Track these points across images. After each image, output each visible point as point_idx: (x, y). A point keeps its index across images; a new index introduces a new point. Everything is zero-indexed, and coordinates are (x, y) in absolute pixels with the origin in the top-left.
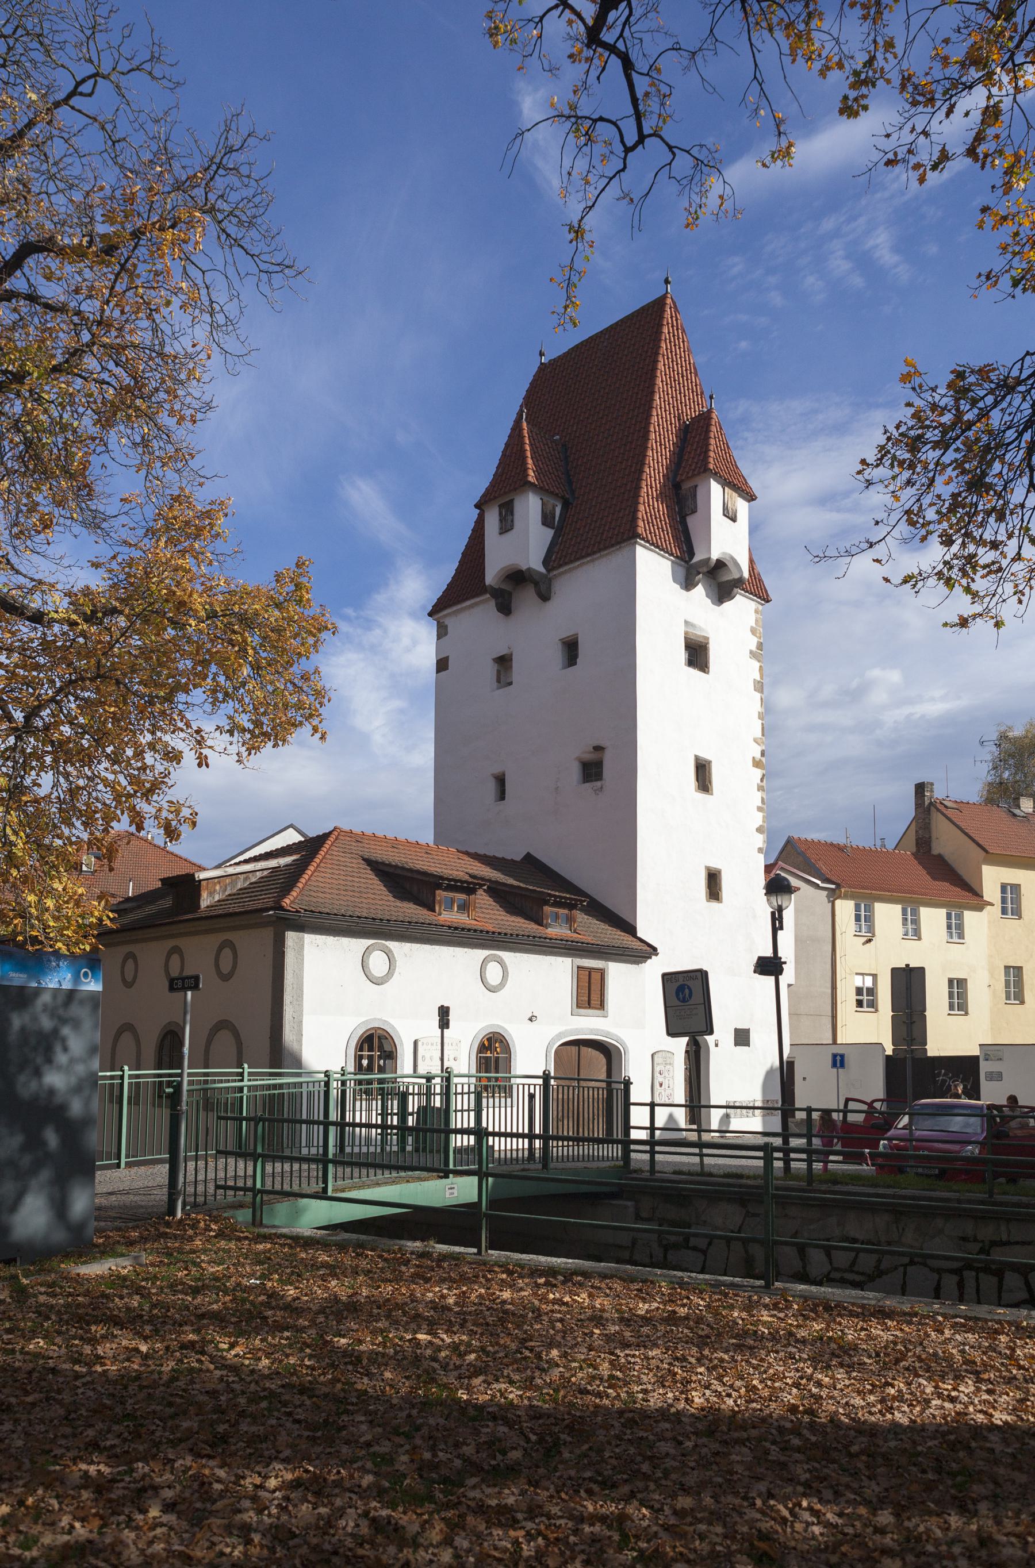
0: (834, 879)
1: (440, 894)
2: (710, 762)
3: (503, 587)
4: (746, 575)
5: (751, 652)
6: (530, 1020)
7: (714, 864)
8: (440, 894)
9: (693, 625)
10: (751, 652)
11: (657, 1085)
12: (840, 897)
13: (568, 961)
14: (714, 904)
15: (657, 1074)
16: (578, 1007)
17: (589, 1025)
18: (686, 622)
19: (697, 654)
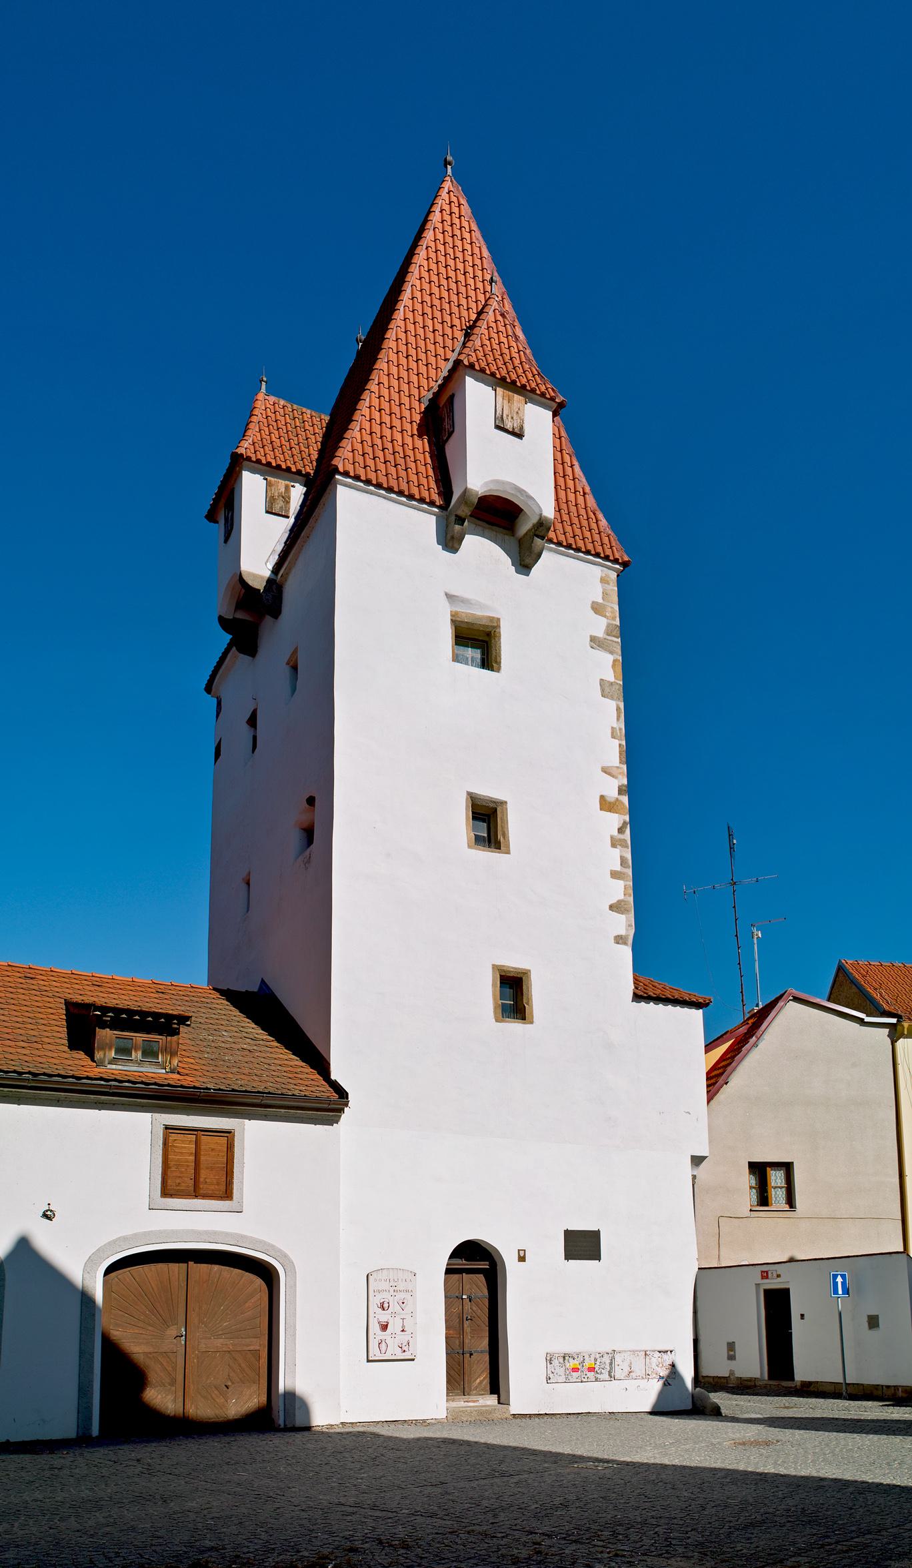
0: (891, 1009)
1: (105, 1035)
2: (503, 803)
3: (240, 615)
4: (549, 512)
5: (593, 639)
6: (45, 1216)
7: (514, 962)
8: (105, 1035)
9: (464, 601)
10: (593, 639)
11: (375, 1328)
12: (902, 1036)
13: (147, 1116)
14: (515, 1027)
15: (374, 1308)
16: (166, 1192)
17: (195, 1224)
18: (448, 596)
19: (478, 641)
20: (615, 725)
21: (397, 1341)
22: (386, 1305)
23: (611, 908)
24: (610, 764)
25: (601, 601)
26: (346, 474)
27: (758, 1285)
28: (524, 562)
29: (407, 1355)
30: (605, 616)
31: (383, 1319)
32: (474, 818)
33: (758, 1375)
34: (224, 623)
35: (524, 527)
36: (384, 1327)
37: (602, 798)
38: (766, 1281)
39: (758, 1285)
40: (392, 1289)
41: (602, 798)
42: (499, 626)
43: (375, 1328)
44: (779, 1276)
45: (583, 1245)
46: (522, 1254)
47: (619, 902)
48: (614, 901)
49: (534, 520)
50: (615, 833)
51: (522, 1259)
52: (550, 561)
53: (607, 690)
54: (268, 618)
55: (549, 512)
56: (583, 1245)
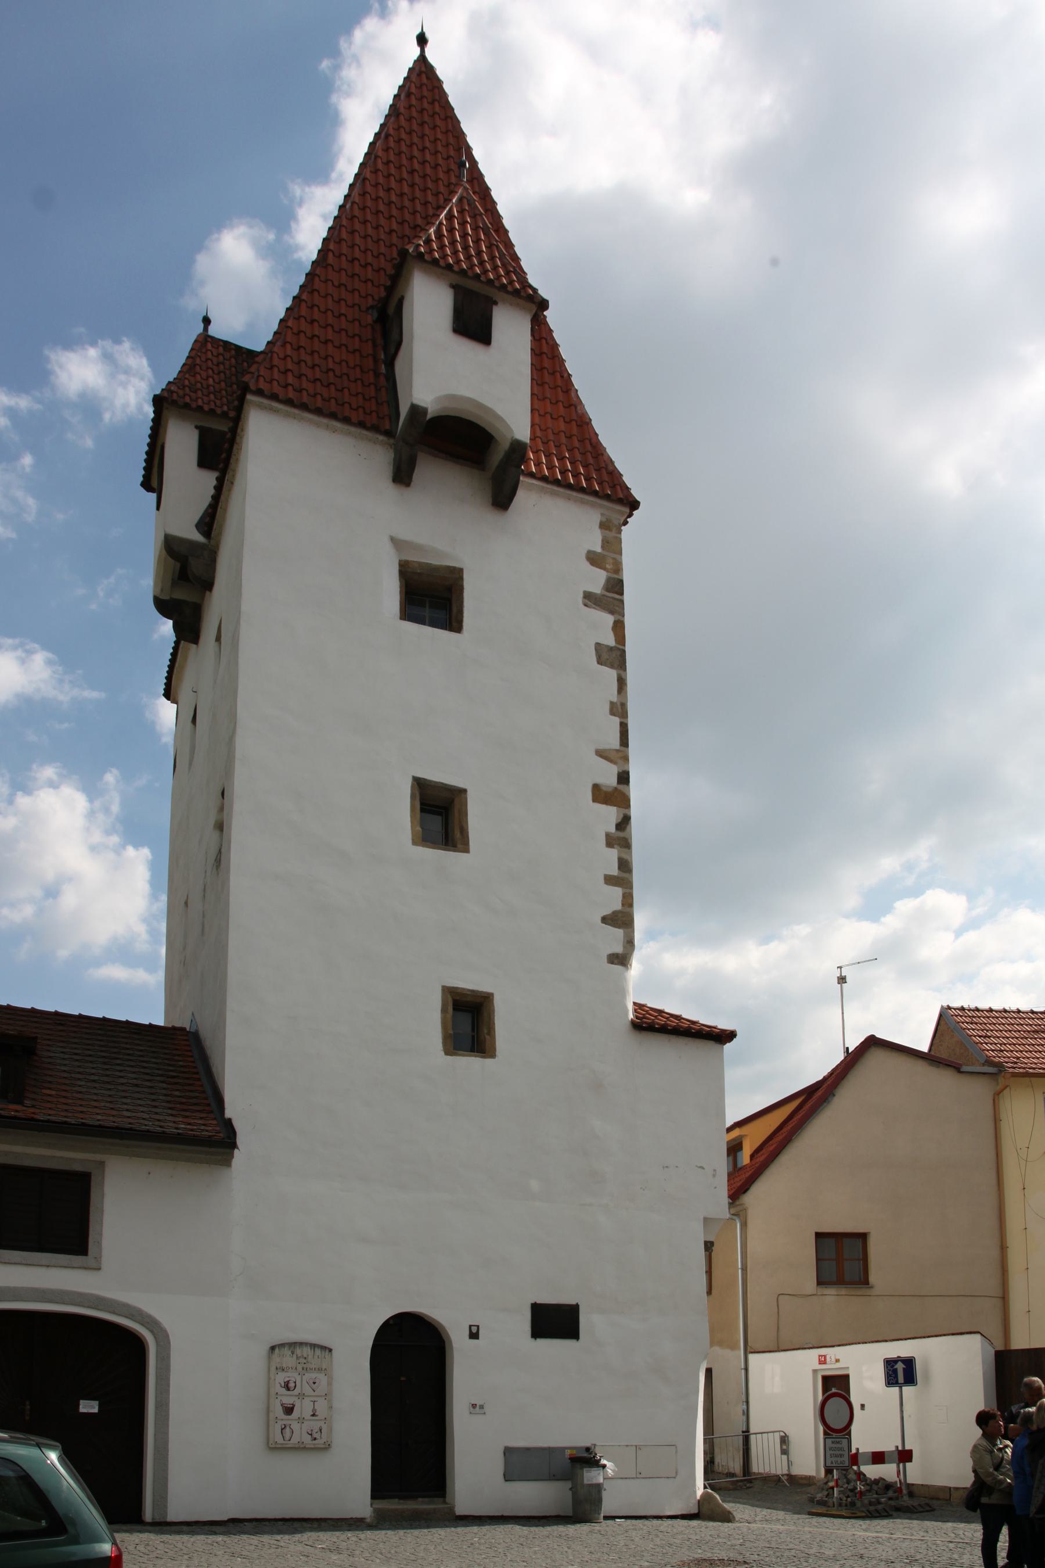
4: (522, 431)
14: (469, 1064)
19: (432, 597)
20: (615, 700)
21: (306, 1427)
22: (292, 1385)
23: (604, 920)
24: (607, 747)
25: (599, 550)
26: (260, 393)
27: (815, 1371)
28: (502, 499)
29: (319, 1442)
30: (605, 569)
31: (288, 1401)
32: (422, 810)
33: (813, 1473)
34: (164, 607)
35: (496, 457)
36: (289, 1410)
37: (596, 788)
38: (823, 1366)
39: (815, 1371)
40: (300, 1368)
41: (596, 788)
42: (462, 578)
43: (279, 1411)
44: (837, 1361)
45: (555, 1321)
46: (474, 1330)
47: (615, 913)
48: (607, 911)
49: (505, 445)
50: (612, 829)
51: (474, 1335)
52: (530, 499)
53: (605, 656)
54: (208, 593)
55: (522, 431)
56: (555, 1321)
